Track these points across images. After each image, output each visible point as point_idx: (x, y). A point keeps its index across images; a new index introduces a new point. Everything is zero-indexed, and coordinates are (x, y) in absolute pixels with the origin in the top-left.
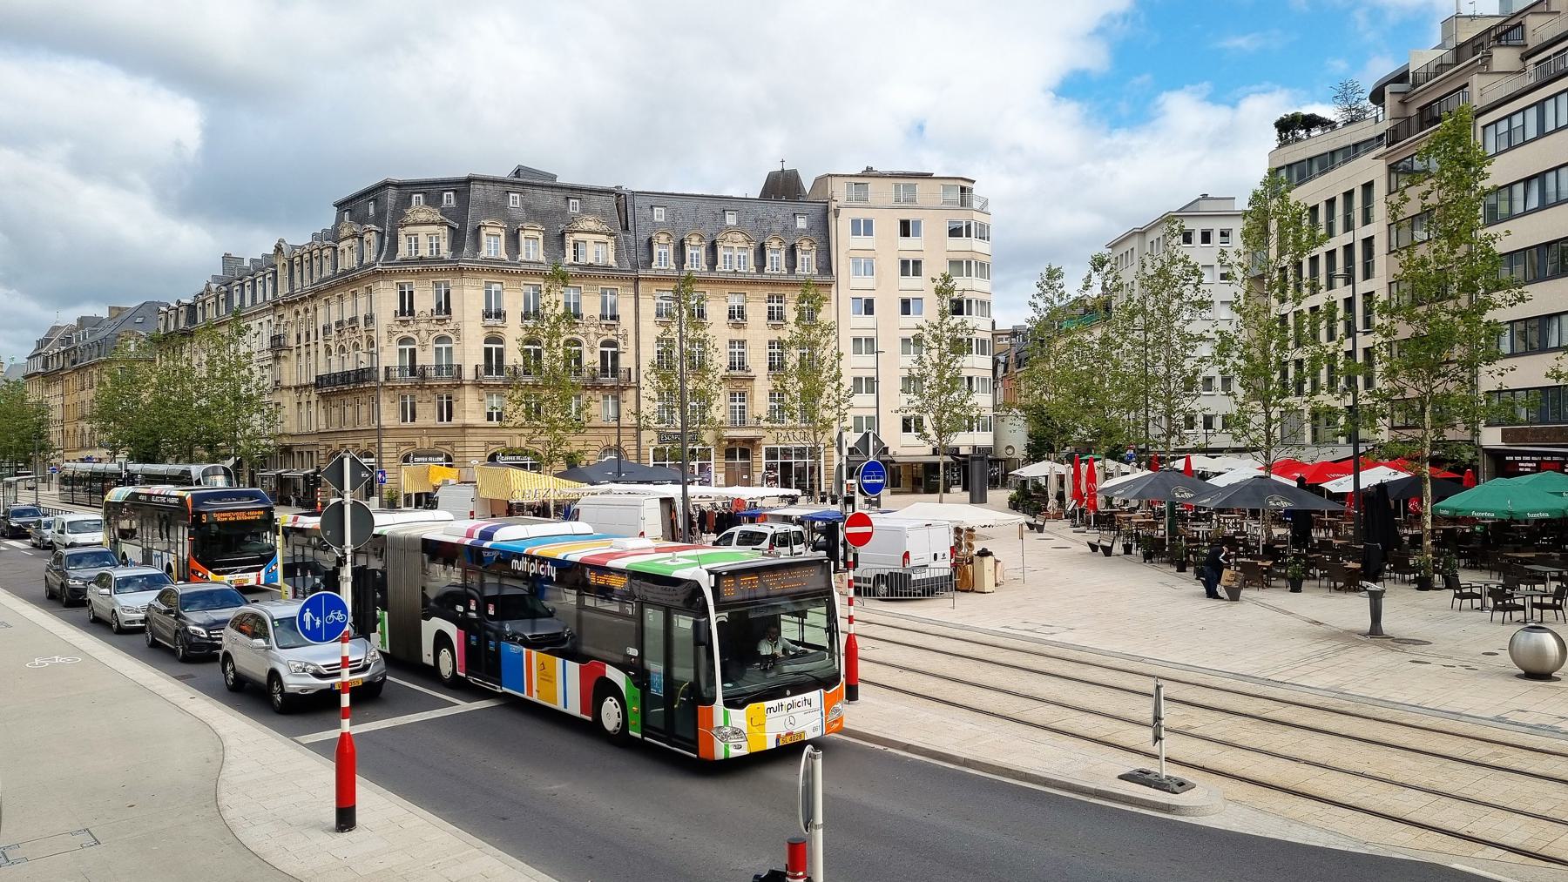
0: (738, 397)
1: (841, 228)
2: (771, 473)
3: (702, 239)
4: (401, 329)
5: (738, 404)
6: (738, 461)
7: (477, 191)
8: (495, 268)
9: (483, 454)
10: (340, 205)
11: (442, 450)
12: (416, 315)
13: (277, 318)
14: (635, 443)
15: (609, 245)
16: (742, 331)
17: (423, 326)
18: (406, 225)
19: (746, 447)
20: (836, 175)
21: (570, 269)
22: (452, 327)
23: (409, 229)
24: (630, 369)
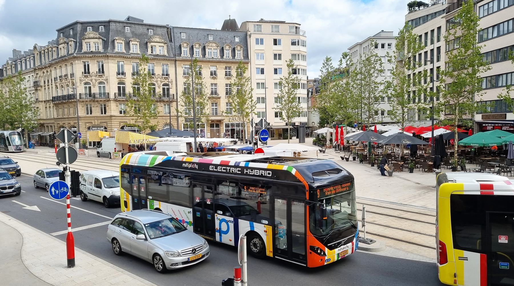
0: (214, 105)
1: (252, 41)
2: (227, 133)
4: (85, 79)
6: (215, 128)
7: (113, 26)
8: (121, 56)
10: (59, 31)
12: (91, 74)
13: (35, 74)
14: (176, 122)
15: (165, 47)
17: (93, 78)
18: (85, 39)
19: (218, 123)
20: (250, 22)
21: (150, 56)
22: (105, 78)
23: (86, 40)
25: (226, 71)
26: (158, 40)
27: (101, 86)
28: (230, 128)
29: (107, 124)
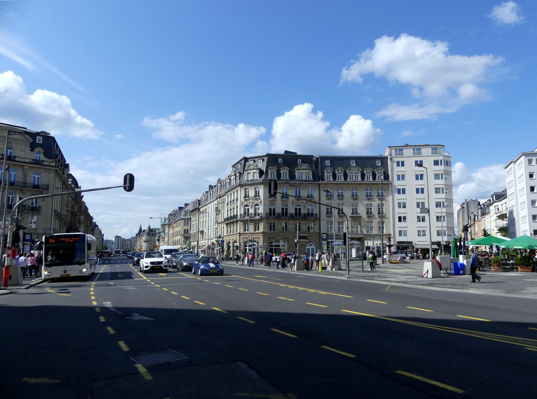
3: (331, 170)
4: (246, 202)
5: (355, 207)
9: (268, 241)
10: (233, 167)
11: (256, 240)
14: (319, 239)
16: (356, 201)
23: (300, 171)
24: (317, 214)
25: (352, 192)
26: (304, 167)
27: (284, 208)
28: (274, 248)
29: (259, 239)
